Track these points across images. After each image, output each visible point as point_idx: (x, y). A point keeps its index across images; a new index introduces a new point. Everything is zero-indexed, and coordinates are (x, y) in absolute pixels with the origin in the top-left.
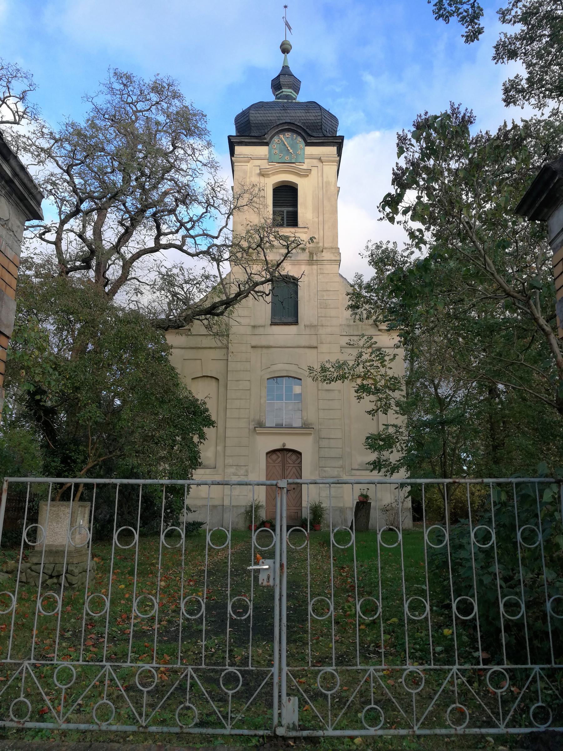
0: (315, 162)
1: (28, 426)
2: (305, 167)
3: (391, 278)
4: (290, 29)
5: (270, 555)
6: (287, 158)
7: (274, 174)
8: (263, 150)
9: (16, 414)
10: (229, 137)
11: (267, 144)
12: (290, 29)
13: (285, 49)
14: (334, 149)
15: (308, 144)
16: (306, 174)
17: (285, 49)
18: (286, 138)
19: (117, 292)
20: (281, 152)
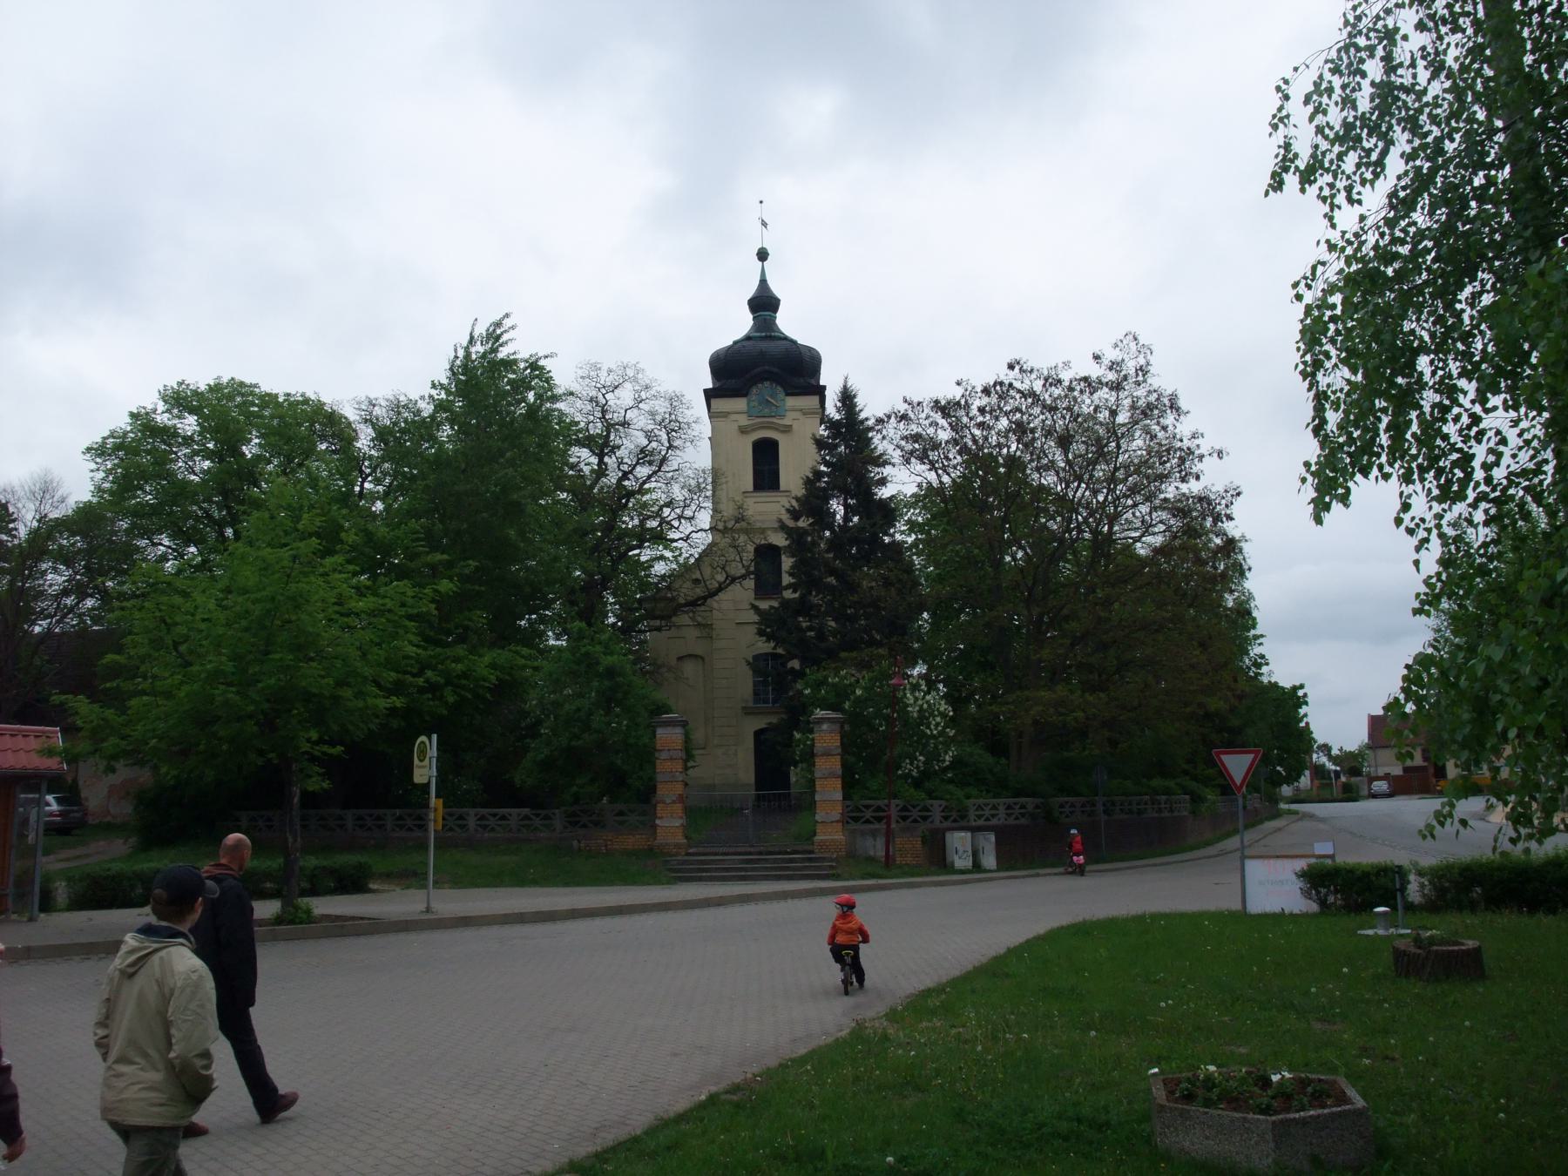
2: (786, 422)
8: (740, 404)
10: (706, 392)
11: (745, 395)
13: (763, 255)
15: (788, 394)
16: (787, 429)
17: (763, 255)
18: (765, 388)
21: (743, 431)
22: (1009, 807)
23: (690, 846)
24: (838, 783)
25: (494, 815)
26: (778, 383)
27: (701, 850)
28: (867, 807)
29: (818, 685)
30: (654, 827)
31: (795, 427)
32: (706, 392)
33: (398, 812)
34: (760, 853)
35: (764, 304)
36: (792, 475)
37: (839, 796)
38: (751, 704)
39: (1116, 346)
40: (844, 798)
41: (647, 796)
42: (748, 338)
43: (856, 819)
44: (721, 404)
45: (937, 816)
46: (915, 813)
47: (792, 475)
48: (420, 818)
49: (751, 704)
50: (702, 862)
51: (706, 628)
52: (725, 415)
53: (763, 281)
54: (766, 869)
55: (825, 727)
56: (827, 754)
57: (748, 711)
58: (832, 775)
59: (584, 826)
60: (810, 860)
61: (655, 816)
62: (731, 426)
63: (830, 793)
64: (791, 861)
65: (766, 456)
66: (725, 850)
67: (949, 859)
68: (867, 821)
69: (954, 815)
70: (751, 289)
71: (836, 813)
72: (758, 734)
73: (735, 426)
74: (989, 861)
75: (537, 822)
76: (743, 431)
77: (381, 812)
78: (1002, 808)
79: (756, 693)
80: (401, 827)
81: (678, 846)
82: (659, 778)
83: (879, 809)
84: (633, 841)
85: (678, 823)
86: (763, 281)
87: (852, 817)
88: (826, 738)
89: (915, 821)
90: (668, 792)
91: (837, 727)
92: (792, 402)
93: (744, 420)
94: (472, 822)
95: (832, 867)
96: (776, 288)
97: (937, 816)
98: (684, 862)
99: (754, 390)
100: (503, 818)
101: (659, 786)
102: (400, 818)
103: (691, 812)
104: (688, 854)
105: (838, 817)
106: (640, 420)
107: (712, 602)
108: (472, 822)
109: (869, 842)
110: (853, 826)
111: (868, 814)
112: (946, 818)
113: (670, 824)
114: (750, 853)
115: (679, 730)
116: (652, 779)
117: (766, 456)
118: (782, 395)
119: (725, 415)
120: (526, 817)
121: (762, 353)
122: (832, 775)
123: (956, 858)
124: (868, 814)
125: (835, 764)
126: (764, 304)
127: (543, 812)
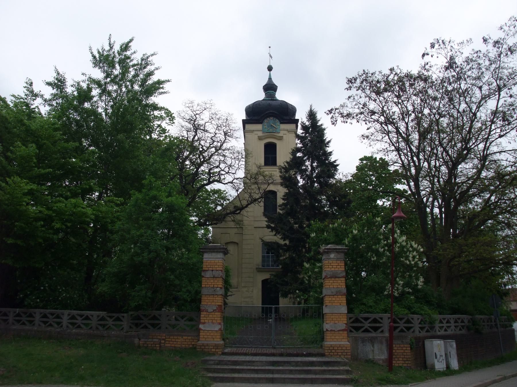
0: (285, 132)
1: (202, 321)
2: (280, 135)
3: (345, 195)
4: (271, 57)
5: (271, 318)
6: (271, 130)
7: (265, 138)
8: (259, 127)
9: (112, 107)
10: (243, 120)
11: (261, 123)
12: (271, 57)
13: (270, 69)
14: (295, 125)
15: (281, 123)
16: (281, 138)
17: (270, 69)
18: (270, 121)
19: (265, 215)
20: (268, 127)
21: (260, 138)
22: (456, 322)
23: (225, 346)
24: (344, 300)
25: (81, 316)
26: (277, 118)
27: (234, 350)
28: (366, 319)
29: (322, 231)
30: (199, 330)
31: (285, 136)
32: (243, 120)
33: (18, 310)
34: (281, 355)
35: (270, 88)
36: (283, 157)
37: (344, 309)
38: (261, 267)
39: (501, 28)
40: (348, 312)
41: (195, 303)
42: (263, 100)
43: (357, 329)
44: (249, 127)
45: (416, 326)
46: (402, 325)
47: (283, 157)
48: (31, 316)
49: (261, 267)
50: (235, 363)
51: (239, 224)
52: (252, 131)
53: (270, 79)
54: (291, 372)
55: (332, 256)
56: (334, 276)
57: (259, 270)
58: (338, 293)
59: (145, 327)
60: (327, 363)
61: (199, 323)
62: (253, 137)
63: (336, 309)
64: (312, 364)
65: (270, 150)
66: (254, 351)
67: (429, 362)
68: (366, 331)
69: (427, 326)
70: (265, 82)
71: (342, 323)
72: (265, 282)
73: (256, 137)
74: (455, 364)
75: (110, 322)
76: (260, 138)
77: (120, 315)
78: (452, 321)
79: (263, 261)
80: (18, 321)
81: (217, 346)
82: (204, 291)
83: (375, 321)
84: (181, 341)
85: (217, 328)
86: (270, 79)
87: (354, 326)
88: (333, 264)
89: (402, 331)
90: (210, 302)
91: (342, 256)
92: (283, 126)
93: (260, 134)
94: (65, 321)
95: (348, 372)
96: (275, 81)
97: (416, 326)
98: (220, 363)
99: (266, 121)
100: (87, 318)
101: (203, 298)
102: (18, 315)
103: (228, 321)
104: (224, 354)
105: (344, 327)
106: (211, 128)
107: (244, 212)
108: (65, 321)
109: (368, 347)
110: (355, 334)
111: (367, 325)
112: (422, 328)
113: (211, 328)
114: (273, 355)
115: (221, 255)
116: (198, 293)
117: (270, 150)
118: (278, 123)
119: (252, 131)
120: (103, 319)
121: (270, 105)
122: (338, 293)
123: (436, 361)
124: (367, 325)
125: (341, 284)
126: (270, 88)
127: (116, 315)
